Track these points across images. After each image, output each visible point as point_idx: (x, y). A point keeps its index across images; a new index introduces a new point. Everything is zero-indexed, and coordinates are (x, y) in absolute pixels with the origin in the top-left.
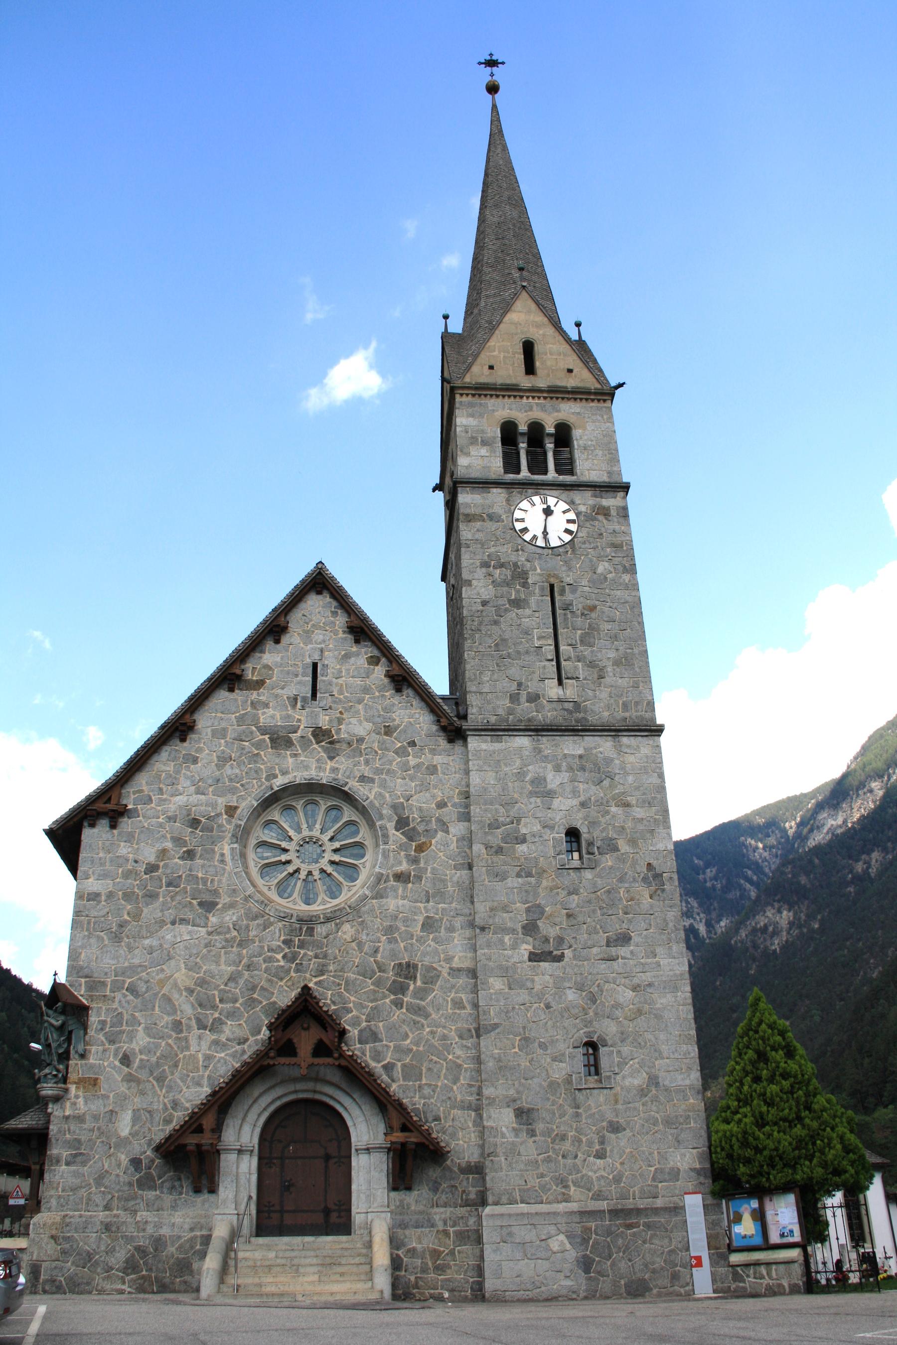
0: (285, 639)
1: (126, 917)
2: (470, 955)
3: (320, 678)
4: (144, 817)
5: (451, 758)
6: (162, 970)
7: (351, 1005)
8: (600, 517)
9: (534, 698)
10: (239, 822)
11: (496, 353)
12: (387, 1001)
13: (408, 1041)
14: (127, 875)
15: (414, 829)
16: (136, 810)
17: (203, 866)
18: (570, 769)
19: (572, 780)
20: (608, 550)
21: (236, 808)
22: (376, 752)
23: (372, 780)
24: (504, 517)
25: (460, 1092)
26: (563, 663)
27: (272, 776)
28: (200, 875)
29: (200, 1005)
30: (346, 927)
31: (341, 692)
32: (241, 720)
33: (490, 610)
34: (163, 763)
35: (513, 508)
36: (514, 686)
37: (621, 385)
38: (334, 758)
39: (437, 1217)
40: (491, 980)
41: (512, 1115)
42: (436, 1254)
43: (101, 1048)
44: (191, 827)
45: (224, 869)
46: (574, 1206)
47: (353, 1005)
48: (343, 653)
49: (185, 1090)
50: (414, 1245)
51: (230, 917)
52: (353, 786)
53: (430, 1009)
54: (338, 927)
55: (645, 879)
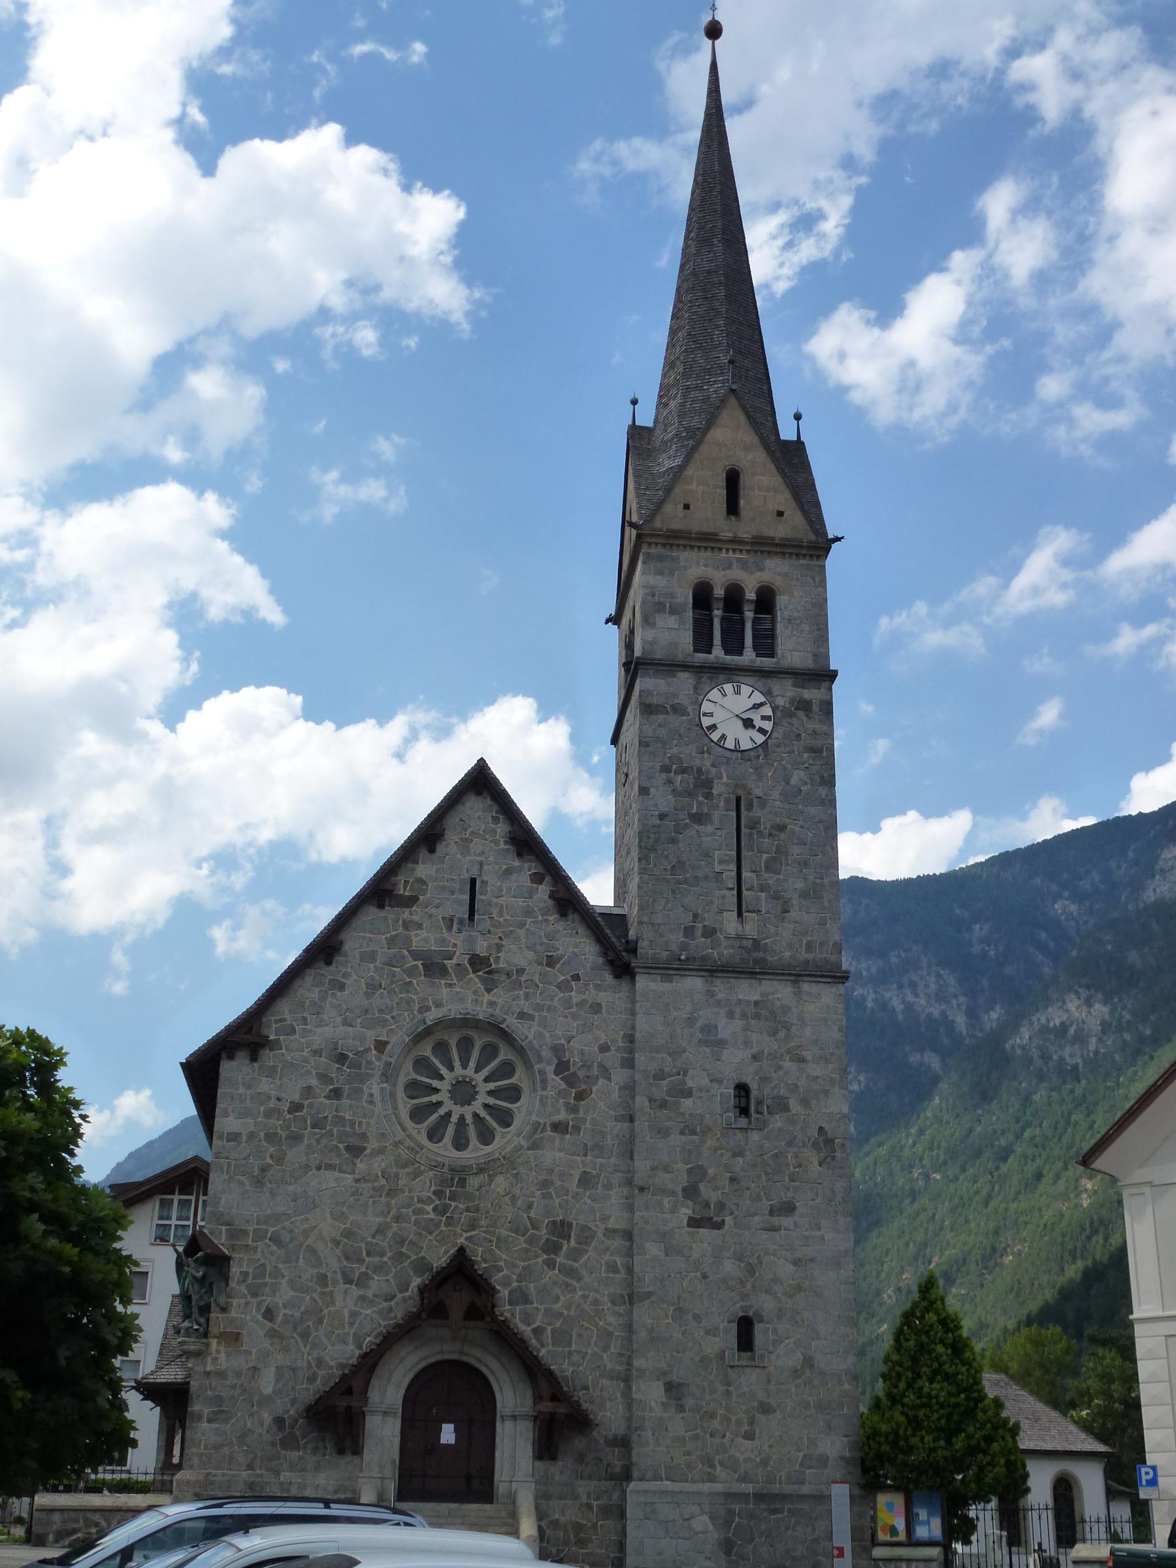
0: (441, 849)
1: (269, 1160)
2: (626, 1215)
3: (478, 897)
4: (287, 1049)
5: (617, 995)
6: (307, 1219)
7: (502, 1263)
8: (801, 714)
9: (710, 932)
10: (390, 1059)
11: (693, 487)
12: (540, 1260)
13: (560, 1305)
14: (269, 1114)
15: (574, 1074)
16: (277, 1041)
17: (351, 1106)
18: (744, 1016)
19: (746, 1029)
20: (806, 755)
21: (386, 1043)
22: (537, 986)
23: (532, 1018)
24: (690, 709)
25: (610, 1362)
26: (745, 893)
27: (424, 1009)
28: (347, 1117)
29: (347, 1258)
30: (500, 1179)
31: (501, 914)
32: (392, 942)
33: (669, 824)
34: (307, 990)
35: (701, 698)
36: (690, 917)
37: (838, 539)
38: (492, 990)
39: (581, 1490)
40: (648, 1245)
41: (662, 1388)
42: (578, 1527)
43: (243, 1301)
44: (338, 1062)
45: (373, 1111)
46: (719, 1487)
47: (505, 1266)
48: (504, 867)
49: (329, 1347)
50: (557, 1516)
51: (378, 1164)
52: (511, 1022)
53: (583, 1272)
54: (491, 1178)
55: (815, 1145)
